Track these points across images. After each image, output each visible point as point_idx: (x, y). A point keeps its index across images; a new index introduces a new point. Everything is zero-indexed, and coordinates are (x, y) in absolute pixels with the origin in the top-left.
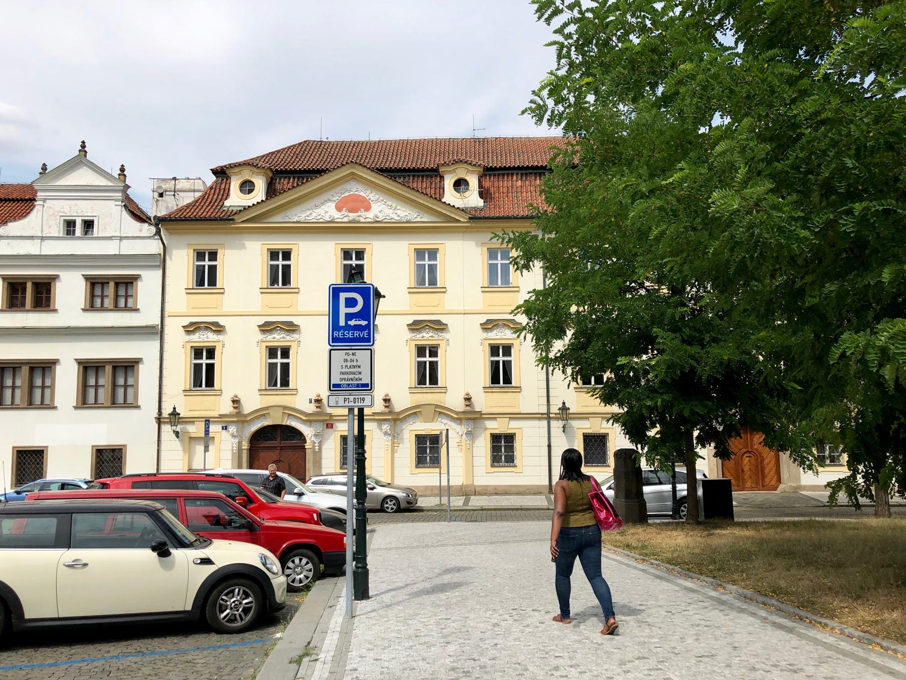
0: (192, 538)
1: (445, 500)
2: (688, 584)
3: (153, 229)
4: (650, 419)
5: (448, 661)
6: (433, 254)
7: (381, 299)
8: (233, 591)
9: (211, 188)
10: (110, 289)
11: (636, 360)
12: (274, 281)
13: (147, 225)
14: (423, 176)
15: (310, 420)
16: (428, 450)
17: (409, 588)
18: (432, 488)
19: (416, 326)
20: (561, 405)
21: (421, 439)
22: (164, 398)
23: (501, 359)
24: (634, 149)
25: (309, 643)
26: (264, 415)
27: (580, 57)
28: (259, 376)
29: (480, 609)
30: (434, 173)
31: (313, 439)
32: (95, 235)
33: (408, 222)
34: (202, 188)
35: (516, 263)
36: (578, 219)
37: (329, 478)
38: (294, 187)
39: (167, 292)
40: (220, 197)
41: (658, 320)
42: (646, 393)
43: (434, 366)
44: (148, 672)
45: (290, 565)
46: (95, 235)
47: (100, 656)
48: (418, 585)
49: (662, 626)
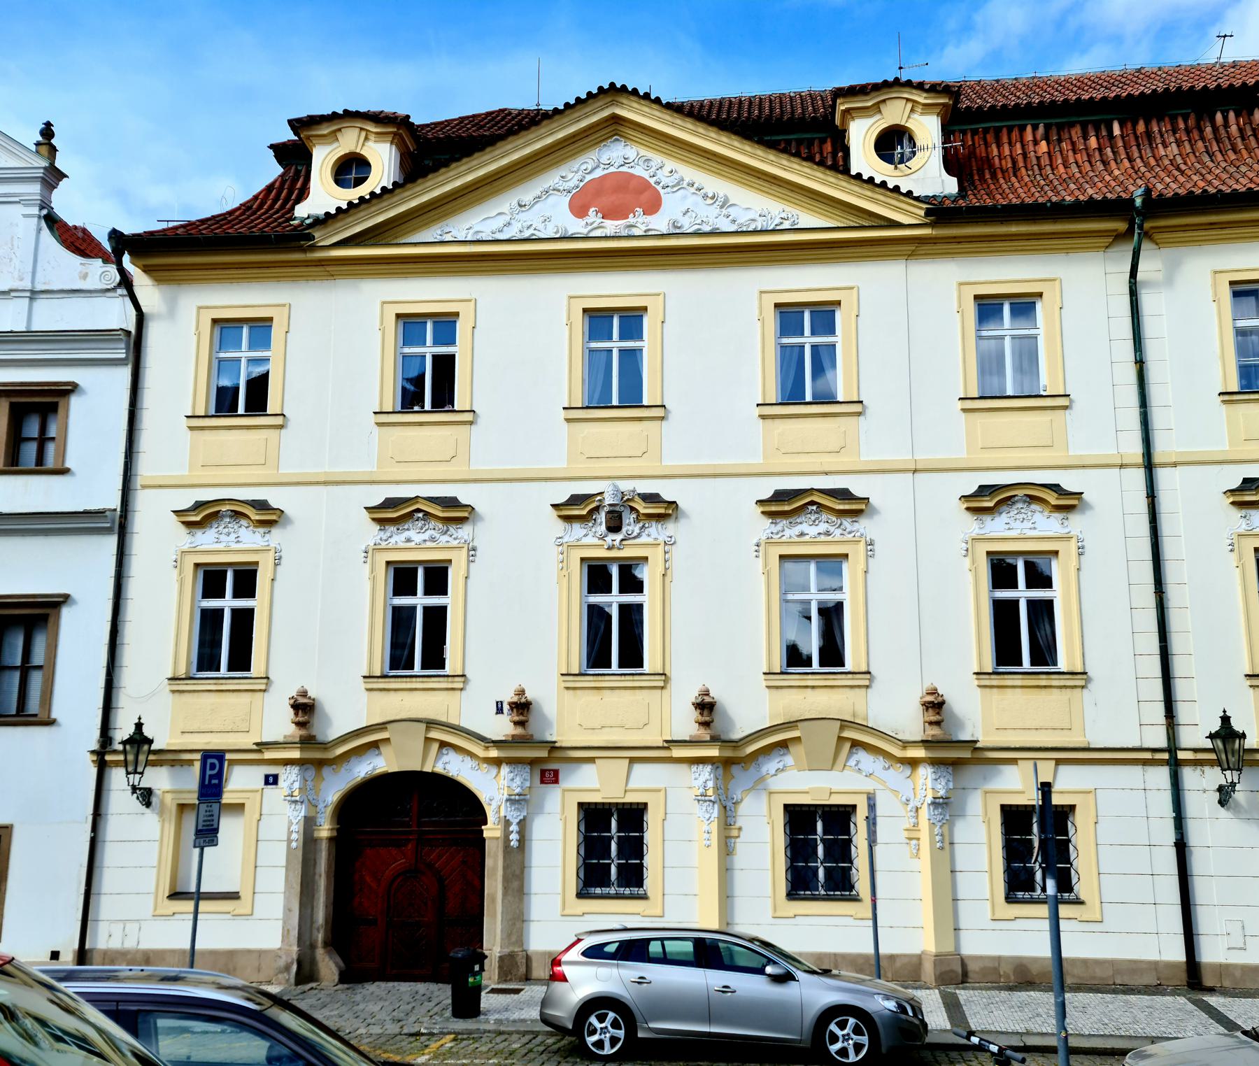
20: (1216, 726)
21: (799, 819)
22: (1181, 689)
23: (228, 603)
28: (368, 639)
43: (632, 616)
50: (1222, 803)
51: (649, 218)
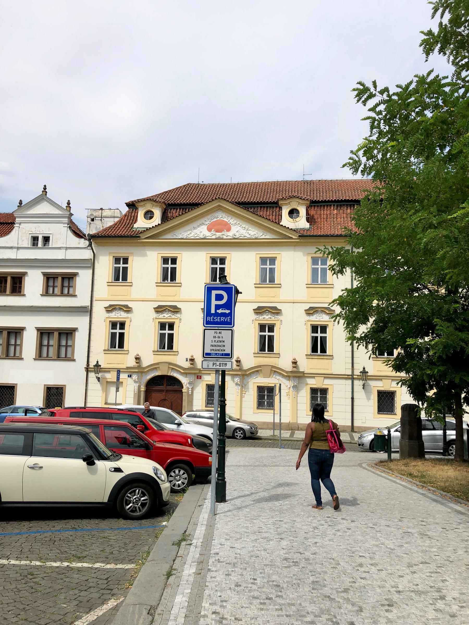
0: (109, 453)
1: (277, 432)
2: (458, 508)
3: (87, 243)
4: (429, 383)
5: (282, 552)
6: (273, 260)
7: (239, 295)
8: (135, 491)
9: (125, 215)
10: (59, 282)
11: (420, 341)
12: (165, 278)
13: (83, 240)
14: (267, 207)
15: (186, 372)
16: (266, 397)
17: (253, 496)
18: (268, 423)
19: (259, 311)
20: (362, 370)
21: (261, 389)
22: (91, 355)
24: (425, 192)
25: (185, 531)
26: (156, 368)
27: (387, 128)
28: (154, 342)
29: (304, 515)
30: (275, 205)
31: (188, 385)
32: (50, 246)
33: (256, 239)
34: (119, 215)
35: (334, 269)
36: (379, 239)
37: (198, 413)
38: (180, 215)
39: (95, 284)
40: (131, 221)
41: (437, 313)
42: (427, 365)
43: (271, 339)
44: (79, 543)
45: (173, 474)
46: (50, 246)
47: (48, 529)
48: (260, 494)
49: (439, 539)
50: (363, 388)
51: (228, 233)
